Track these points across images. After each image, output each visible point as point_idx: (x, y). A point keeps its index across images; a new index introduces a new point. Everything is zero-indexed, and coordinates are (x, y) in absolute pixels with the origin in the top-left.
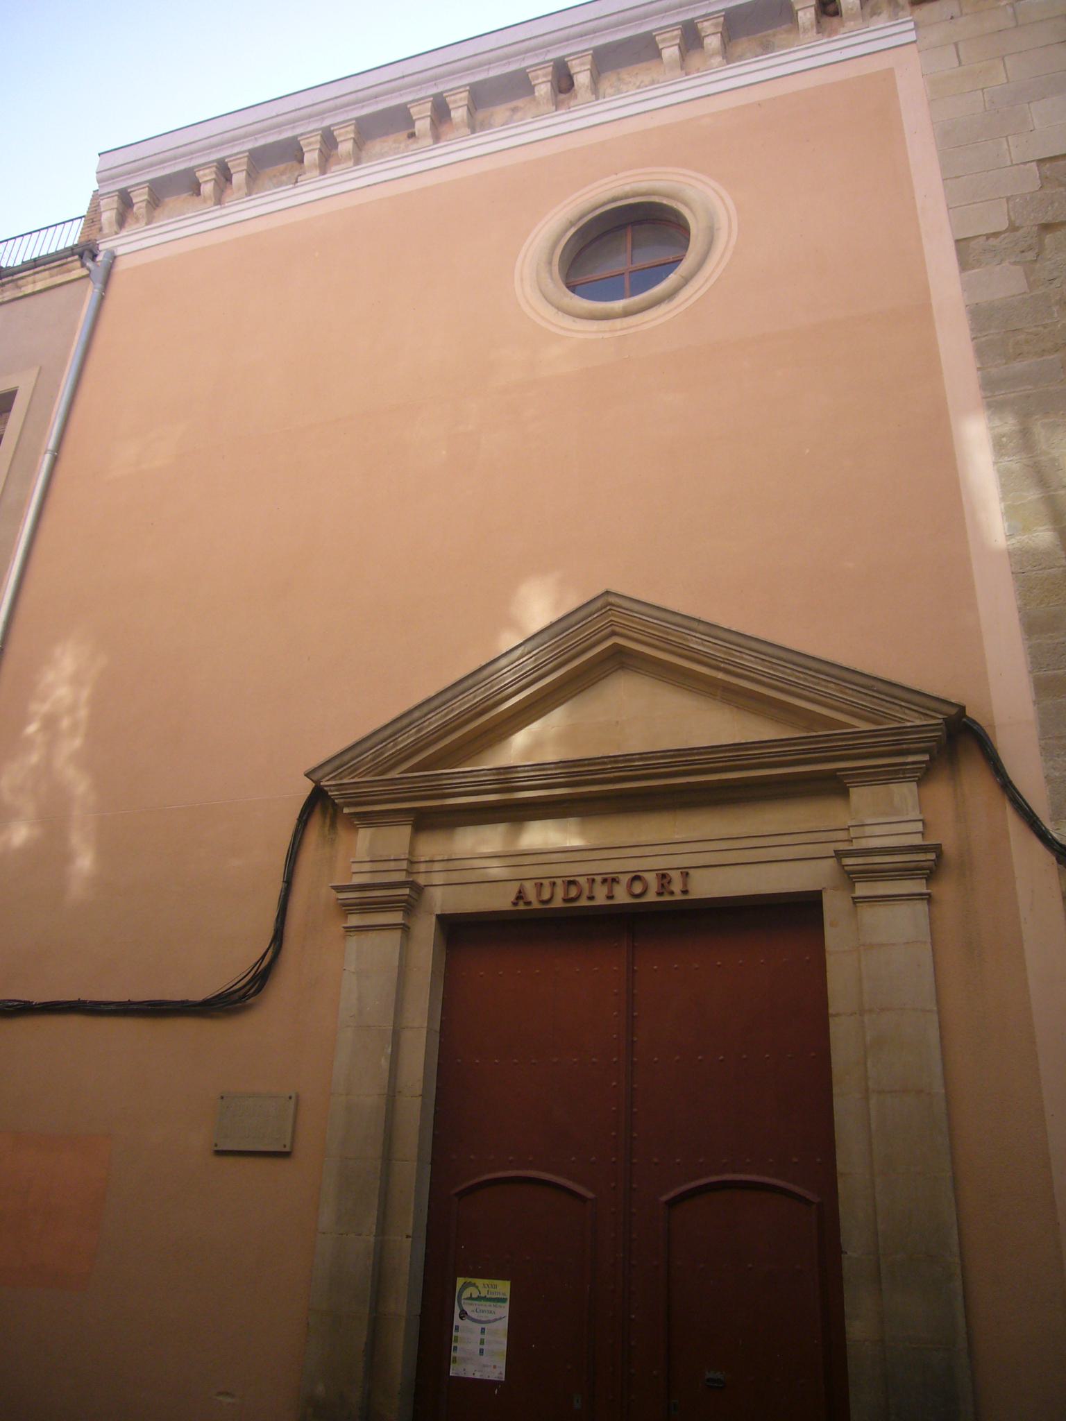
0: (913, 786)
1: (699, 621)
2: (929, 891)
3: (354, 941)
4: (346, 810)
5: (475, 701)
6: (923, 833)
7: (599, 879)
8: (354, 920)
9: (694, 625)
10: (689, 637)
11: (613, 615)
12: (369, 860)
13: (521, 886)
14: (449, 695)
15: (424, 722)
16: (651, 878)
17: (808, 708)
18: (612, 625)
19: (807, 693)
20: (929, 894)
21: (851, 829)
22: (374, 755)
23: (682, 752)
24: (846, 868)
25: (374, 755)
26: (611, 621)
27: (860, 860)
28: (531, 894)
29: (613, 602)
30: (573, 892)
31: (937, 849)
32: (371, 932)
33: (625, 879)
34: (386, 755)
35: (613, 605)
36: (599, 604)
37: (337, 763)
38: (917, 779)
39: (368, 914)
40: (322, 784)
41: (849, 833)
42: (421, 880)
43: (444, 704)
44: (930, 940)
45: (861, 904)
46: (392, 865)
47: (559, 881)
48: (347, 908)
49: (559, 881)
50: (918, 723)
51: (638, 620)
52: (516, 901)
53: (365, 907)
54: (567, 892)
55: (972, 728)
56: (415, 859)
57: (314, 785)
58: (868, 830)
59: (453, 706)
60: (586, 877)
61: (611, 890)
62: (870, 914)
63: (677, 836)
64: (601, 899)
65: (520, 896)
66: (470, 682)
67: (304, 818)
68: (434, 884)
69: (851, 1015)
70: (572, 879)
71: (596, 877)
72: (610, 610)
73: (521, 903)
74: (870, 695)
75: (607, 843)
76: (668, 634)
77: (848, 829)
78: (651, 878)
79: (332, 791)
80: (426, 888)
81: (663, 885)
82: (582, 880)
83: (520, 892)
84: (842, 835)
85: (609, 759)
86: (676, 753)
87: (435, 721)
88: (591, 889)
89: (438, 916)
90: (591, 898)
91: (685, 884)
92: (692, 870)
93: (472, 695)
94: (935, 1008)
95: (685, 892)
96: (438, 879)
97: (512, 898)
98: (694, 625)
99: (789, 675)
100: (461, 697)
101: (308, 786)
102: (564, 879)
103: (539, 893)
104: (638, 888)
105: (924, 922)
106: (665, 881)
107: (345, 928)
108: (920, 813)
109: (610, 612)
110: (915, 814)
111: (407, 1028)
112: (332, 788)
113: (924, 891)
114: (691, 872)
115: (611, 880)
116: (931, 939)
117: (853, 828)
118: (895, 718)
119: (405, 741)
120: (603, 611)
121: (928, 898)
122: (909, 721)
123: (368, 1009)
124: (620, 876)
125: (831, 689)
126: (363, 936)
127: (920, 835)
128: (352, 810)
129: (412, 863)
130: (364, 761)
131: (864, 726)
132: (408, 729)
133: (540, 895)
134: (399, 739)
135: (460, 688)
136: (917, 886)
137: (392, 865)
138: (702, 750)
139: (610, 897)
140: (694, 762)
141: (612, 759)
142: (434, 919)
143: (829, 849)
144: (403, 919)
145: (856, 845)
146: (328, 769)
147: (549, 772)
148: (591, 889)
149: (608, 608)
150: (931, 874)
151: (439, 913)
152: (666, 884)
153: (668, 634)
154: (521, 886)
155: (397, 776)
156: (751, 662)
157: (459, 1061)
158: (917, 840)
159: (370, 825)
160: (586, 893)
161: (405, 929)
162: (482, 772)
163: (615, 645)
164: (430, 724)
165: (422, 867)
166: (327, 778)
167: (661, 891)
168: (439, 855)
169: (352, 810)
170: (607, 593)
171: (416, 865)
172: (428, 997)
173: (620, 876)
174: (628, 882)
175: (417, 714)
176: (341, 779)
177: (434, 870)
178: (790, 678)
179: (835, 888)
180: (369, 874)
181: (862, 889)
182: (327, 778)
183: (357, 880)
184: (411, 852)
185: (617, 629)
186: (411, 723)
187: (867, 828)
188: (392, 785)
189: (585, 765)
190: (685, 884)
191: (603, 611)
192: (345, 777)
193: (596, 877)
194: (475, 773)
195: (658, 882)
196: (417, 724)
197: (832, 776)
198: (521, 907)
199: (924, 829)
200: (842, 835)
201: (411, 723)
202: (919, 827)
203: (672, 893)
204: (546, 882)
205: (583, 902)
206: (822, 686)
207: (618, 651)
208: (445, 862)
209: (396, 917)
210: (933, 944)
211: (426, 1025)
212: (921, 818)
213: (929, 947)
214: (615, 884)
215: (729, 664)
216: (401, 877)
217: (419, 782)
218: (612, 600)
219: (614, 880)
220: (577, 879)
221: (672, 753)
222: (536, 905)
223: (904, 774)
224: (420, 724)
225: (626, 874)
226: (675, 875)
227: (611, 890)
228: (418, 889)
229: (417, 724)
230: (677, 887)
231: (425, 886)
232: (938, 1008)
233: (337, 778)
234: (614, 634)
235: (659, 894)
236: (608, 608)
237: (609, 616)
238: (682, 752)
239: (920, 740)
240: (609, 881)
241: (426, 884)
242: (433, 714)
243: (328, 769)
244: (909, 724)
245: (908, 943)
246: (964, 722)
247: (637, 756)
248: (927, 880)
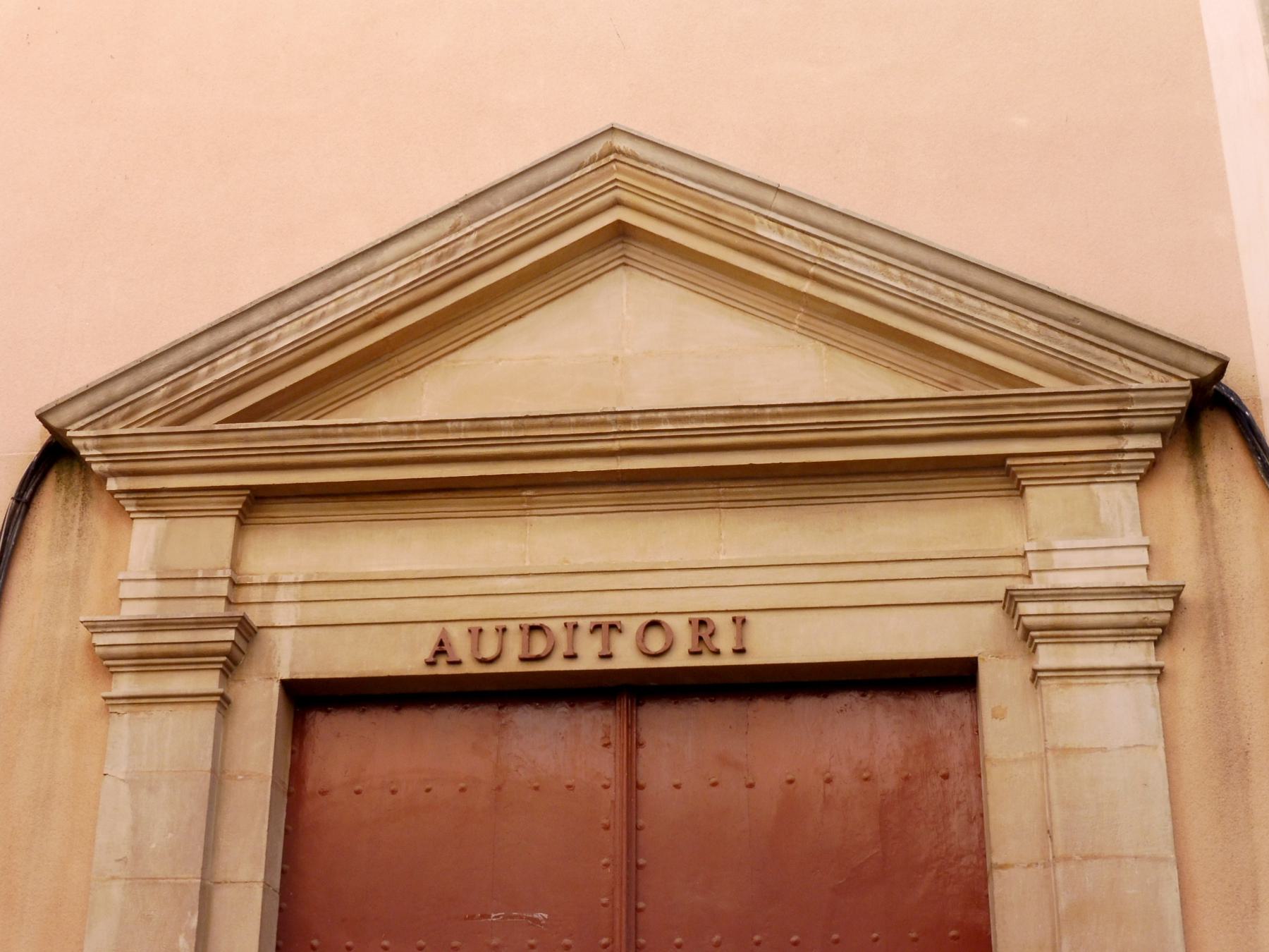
0: (1132, 488)
1: (777, 190)
2: (1161, 663)
3: (123, 725)
4: (112, 484)
5: (366, 302)
6: (1148, 568)
7: (585, 624)
8: (125, 685)
9: (768, 196)
10: (721, 204)
11: (618, 170)
12: (155, 577)
13: (444, 632)
14: (317, 288)
15: (270, 332)
16: (680, 627)
17: (687, 244)
18: (616, 187)
19: (960, 326)
20: (1161, 668)
21: (1029, 555)
22: (170, 387)
23: (745, 411)
24: (1026, 620)
25: (170, 387)
26: (616, 180)
27: (1049, 608)
28: (461, 646)
29: (622, 148)
30: (539, 646)
31: (1176, 593)
32: (157, 708)
33: (632, 626)
34: (194, 388)
35: (619, 152)
36: (597, 148)
37: (100, 396)
38: (1138, 478)
39: (176, 674)
40: (69, 434)
41: (1025, 564)
42: (255, 617)
43: (308, 303)
44: (1162, 744)
45: (1048, 682)
46: (200, 588)
47: (513, 626)
48: (108, 664)
49: (513, 626)
50: (1147, 384)
51: (665, 182)
52: (432, 660)
53: (145, 661)
54: (528, 645)
55: (1228, 399)
56: (238, 579)
57: (48, 435)
58: (1058, 559)
59: (325, 309)
60: (563, 621)
61: (607, 644)
62: (1058, 697)
63: (722, 557)
64: (588, 660)
65: (441, 649)
66: (358, 267)
67: (27, 496)
68: (277, 624)
69: (1029, 866)
70: (537, 622)
71: (484, 625)
72: (615, 160)
73: (442, 660)
74: (1070, 335)
75: (599, 562)
76: (717, 209)
77: (1024, 556)
78: (680, 627)
79: (85, 448)
80: (265, 631)
81: (701, 638)
82: (555, 626)
83: (441, 643)
84: (1013, 566)
85: (615, 417)
86: (733, 412)
87: (289, 334)
88: (572, 641)
89: (284, 684)
90: (572, 657)
91: (740, 638)
92: (628, 618)
93: (360, 292)
94: (1173, 856)
95: (740, 651)
96: (282, 615)
97: (427, 653)
98: (768, 196)
99: (930, 293)
100: (339, 294)
101: (34, 439)
102: (523, 622)
103: (477, 646)
104: (656, 642)
105: (1153, 714)
106: (704, 632)
107: (105, 698)
108: (1144, 534)
109: (614, 166)
110: (1136, 537)
111: (226, 882)
112: (89, 442)
113: (1153, 662)
114: (750, 617)
115: (608, 628)
116: (1165, 742)
117: (1035, 555)
118: (1109, 375)
119: (229, 365)
120: (603, 162)
121: (1159, 674)
122: (1136, 382)
123: (153, 846)
124: (624, 620)
125: (1004, 320)
126: (142, 715)
127: (1144, 570)
128: (126, 483)
129: (234, 584)
130: (149, 397)
131: (1050, 384)
132: (239, 344)
133: (478, 649)
134: (219, 362)
135: (340, 276)
136: (1138, 654)
137: (200, 588)
138: (780, 410)
139: (607, 657)
140: (764, 429)
141: (620, 417)
142: (276, 688)
143: (997, 589)
144: (220, 687)
145: (1037, 583)
146: (82, 406)
147: (503, 434)
148: (572, 641)
149: (612, 157)
150: (1162, 634)
151: (286, 676)
152: (706, 638)
153: (717, 209)
154: (444, 632)
155: (218, 427)
156: (866, 266)
157: (315, 942)
158: (1138, 578)
159: (158, 514)
160: (562, 649)
161: (224, 703)
162: (380, 428)
163: (619, 222)
164: (278, 339)
165: (255, 594)
166: (80, 424)
167: (699, 649)
168: (287, 574)
169: (126, 483)
170: (612, 130)
171: (244, 590)
172: (266, 827)
173: (624, 620)
174: (637, 633)
175: (256, 318)
176: (105, 427)
177: (276, 600)
178: (933, 299)
179: (999, 655)
180: (155, 603)
181: (1048, 656)
182: (80, 424)
183: (131, 611)
184: (234, 565)
185: (625, 196)
186: (244, 334)
187: (1055, 555)
188: (205, 442)
189: (570, 425)
190: (740, 638)
191: (603, 162)
192: (115, 422)
193: (580, 622)
194: (366, 429)
195: (693, 632)
196: (255, 335)
197: (997, 464)
198: (443, 669)
199: (1150, 562)
200: (1013, 566)
201: (244, 334)
202: (1142, 557)
203: (717, 652)
204: (489, 627)
205: (556, 664)
206: (988, 314)
207: (621, 232)
208: (299, 587)
209: (209, 682)
210: (1168, 751)
211: (261, 877)
212: (1146, 541)
213: (1161, 753)
214: (614, 634)
215: (825, 268)
216: (219, 608)
217: (262, 439)
218: (621, 143)
219: (613, 626)
220: (546, 623)
221: (727, 412)
222: (470, 667)
223: (1119, 467)
224: (260, 337)
225: (634, 618)
226: (722, 623)
227: (607, 644)
228: (247, 631)
229: (255, 335)
230: (725, 640)
231: (259, 628)
232: (1177, 856)
233: (100, 424)
234: (618, 203)
235: (693, 653)
236: (612, 157)
237: (612, 172)
238: (745, 411)
239: (1149, 413)
240: (605, 627)
241: (259, 625)
242: (286, 320)
243: (82, 406)
244: (1135, 386)
245: (1126, 747)
246: (1215, 390)
247: (665, 414)
248: (1156, 643)
